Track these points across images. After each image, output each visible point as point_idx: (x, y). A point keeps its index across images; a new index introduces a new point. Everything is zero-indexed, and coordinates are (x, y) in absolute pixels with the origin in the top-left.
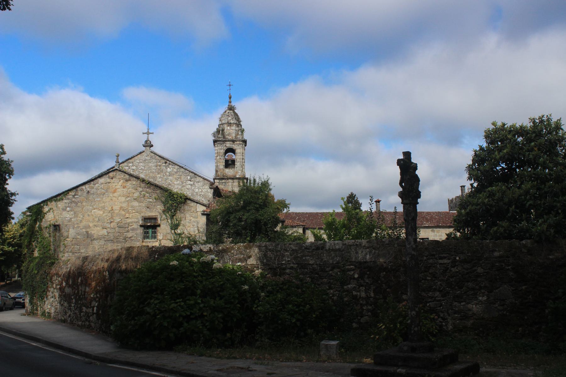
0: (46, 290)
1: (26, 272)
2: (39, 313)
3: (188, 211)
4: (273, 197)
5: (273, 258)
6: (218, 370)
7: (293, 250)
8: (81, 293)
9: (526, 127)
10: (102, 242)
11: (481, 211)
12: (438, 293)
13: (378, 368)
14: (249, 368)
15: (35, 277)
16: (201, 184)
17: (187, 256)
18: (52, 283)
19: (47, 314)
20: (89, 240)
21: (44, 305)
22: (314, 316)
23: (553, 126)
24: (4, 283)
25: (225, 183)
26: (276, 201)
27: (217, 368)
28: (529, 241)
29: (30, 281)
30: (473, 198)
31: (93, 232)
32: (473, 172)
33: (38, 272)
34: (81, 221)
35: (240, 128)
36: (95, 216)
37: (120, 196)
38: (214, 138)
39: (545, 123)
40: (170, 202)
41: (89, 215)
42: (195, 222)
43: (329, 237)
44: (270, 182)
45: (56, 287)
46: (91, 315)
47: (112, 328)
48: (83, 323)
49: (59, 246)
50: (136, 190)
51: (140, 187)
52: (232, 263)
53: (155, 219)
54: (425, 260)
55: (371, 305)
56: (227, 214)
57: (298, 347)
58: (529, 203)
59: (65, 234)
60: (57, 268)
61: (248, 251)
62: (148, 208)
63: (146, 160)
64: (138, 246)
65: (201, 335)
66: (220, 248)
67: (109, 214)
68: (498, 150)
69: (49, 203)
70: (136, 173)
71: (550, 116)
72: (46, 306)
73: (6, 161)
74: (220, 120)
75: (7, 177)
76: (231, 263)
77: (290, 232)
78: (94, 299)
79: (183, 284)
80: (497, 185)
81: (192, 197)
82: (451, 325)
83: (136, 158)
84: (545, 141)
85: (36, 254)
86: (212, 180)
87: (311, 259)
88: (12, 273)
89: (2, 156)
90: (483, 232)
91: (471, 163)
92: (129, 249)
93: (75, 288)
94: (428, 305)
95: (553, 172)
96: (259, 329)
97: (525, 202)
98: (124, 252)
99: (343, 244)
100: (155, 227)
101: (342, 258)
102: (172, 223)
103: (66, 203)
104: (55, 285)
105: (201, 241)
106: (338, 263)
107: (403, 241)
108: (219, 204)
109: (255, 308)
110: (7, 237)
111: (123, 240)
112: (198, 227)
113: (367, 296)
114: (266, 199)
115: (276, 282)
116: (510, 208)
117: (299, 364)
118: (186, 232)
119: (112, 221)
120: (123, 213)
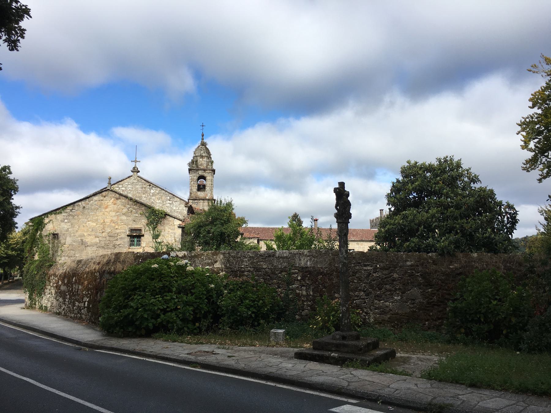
0: (44, 288)
1: (27, 272)
2: (37, 307)
3: (167, 224)
4: (235, 214)
5: (235, 263)
6: (188, 354)
7: (250, 257)
8: (75, 291)
9: (434, 165)
10: (95, 248)
11: (397, 229)
12: (363, 293)
13: (316, 352)
14: (213, 351)
15: (35, 277)
16: (177, 203)
17: (165, 260)
18: (50, 282)
19: (44, 308)
20: (83, 246)
21: (42, 300)
22: (266, 309)
23: (455, 165)
24: (7, 281)
25: (197, 203)
26: (236, 218)
27: (186, 352)
28: (434, 254)
29: (30, 280)
30: (391, 219)
31: (87, 240)
32: (391, 199)
33: (38, 273)
34: (77, 231)
35: (210, 160)
36: (89, 227)
37: (111, 211)
38: (189, 167)
39: (449, 162)
40: (153, 217)
41: (84, 226)
42: (172, 233)
43: (279, 247)
44: (233, 203)
45: (53, 285)
46: (82, 309)
47: (100, 319)
48: (75, 315)
49: (57, 251)
50: (125, 206)
51: (128, 204)
52: (202, 266)
53: (140, 230)
54: (353, 267)
55: (310, 301)
56: (199, 227)
57: (253, 334)
58: (434, 224)
59: (63, 241)
60: (55, 270)
61: (215, 257)
62: (134, 221)
63: (133, 183)
64: (125, 252)
65: (175, 325)
66: (193, 254)
67: (102, 226)
68: (411, 182)
69: (49, 216)
70: (125, 193)
71: (453, 156)
72: (43, 301)
73: (12, 180)
74: (195, 153)
75: (13, 193)
76: (201, 267)
77: (247, 242)
78: (86, 295)
79: (162, 283)
80: (410, 210)
81: (170, 214)
82: (373, 319)
83: (125, 181)
84: (448, 176)
85: (36, 257)
86: (187, 201)
87: (264, 265)
88: (14, 273)
89: (8, 175)
90: (398, 246)
91: (390, 192)
92: (118, 255)
93: (69, 286)
94: (355, 302)
95: (454, 201)
96: (222, 320)
97: (432, 223)
98: (114, 257)
99: (290, 253)
100: (140, 236)
101: (289, 264)
102: (154, 234)
103: (64, 216)
104: (52, 283)
105: (177, 249)
106: (285, 267)
107: (336, 251)
108: (192, 219)
109: (219, 302)
110: (11, 243)
111: (113, 247)
112: (175, 237)
113: (307, 294)
114: (230, 216)
115: (236, 282)
116: (419, 228)
117: (253, 348)
118: (165, 241)
119: (104, 231)
120: (113, 225)
